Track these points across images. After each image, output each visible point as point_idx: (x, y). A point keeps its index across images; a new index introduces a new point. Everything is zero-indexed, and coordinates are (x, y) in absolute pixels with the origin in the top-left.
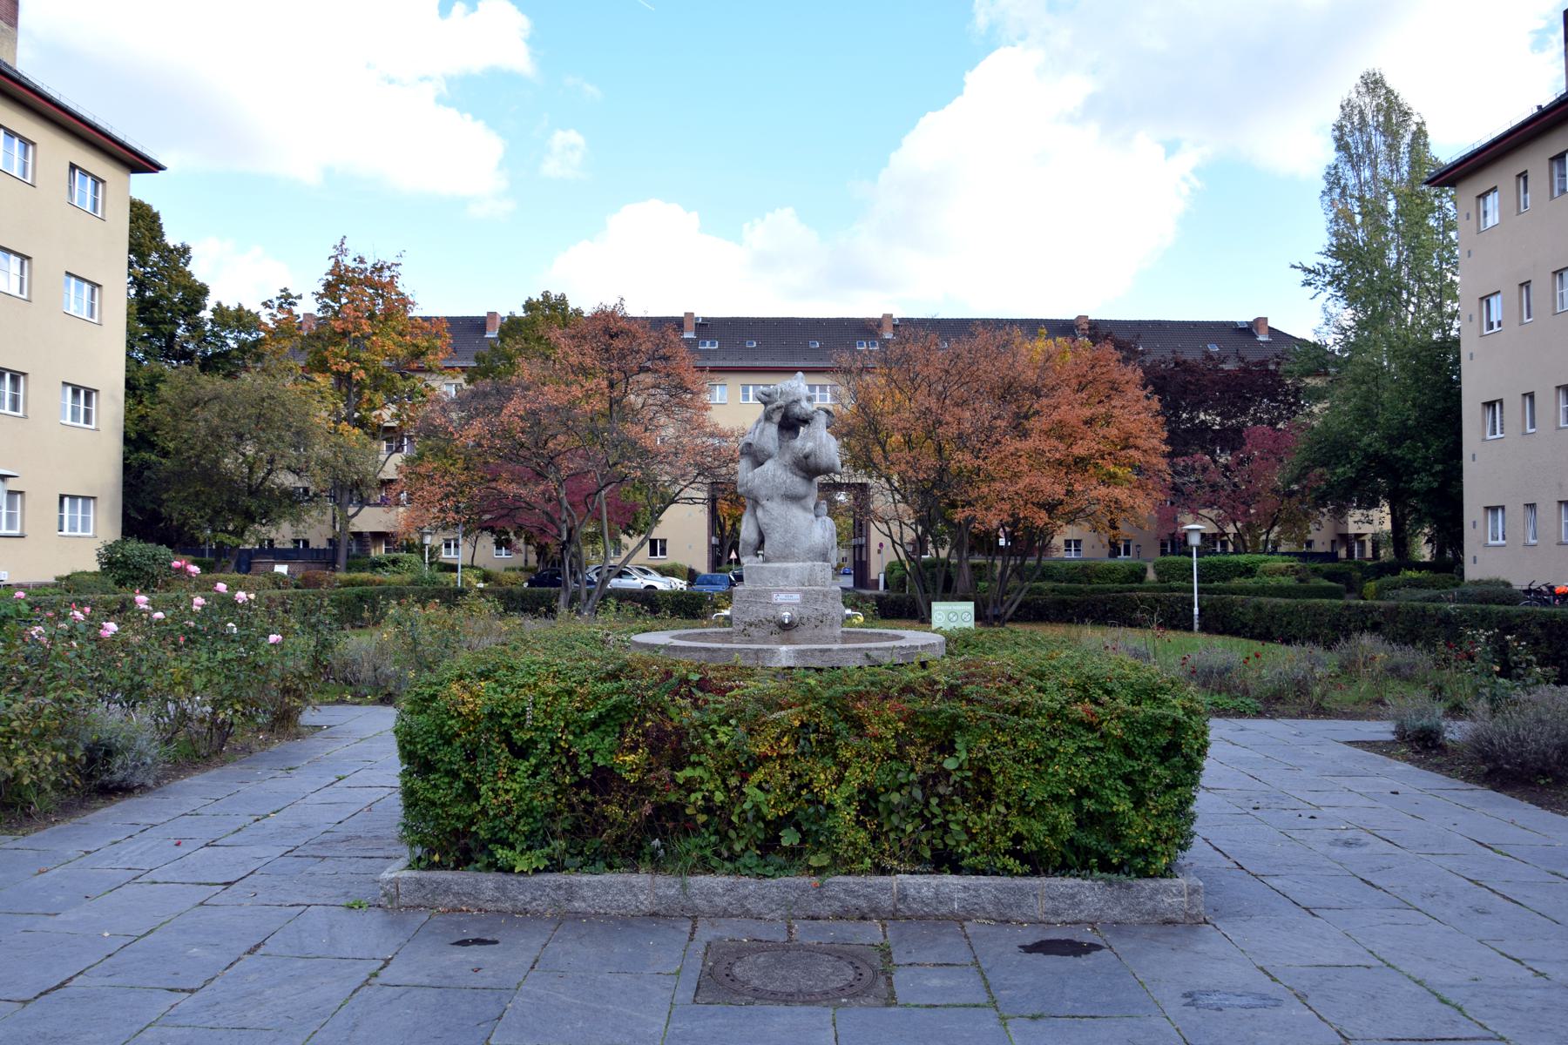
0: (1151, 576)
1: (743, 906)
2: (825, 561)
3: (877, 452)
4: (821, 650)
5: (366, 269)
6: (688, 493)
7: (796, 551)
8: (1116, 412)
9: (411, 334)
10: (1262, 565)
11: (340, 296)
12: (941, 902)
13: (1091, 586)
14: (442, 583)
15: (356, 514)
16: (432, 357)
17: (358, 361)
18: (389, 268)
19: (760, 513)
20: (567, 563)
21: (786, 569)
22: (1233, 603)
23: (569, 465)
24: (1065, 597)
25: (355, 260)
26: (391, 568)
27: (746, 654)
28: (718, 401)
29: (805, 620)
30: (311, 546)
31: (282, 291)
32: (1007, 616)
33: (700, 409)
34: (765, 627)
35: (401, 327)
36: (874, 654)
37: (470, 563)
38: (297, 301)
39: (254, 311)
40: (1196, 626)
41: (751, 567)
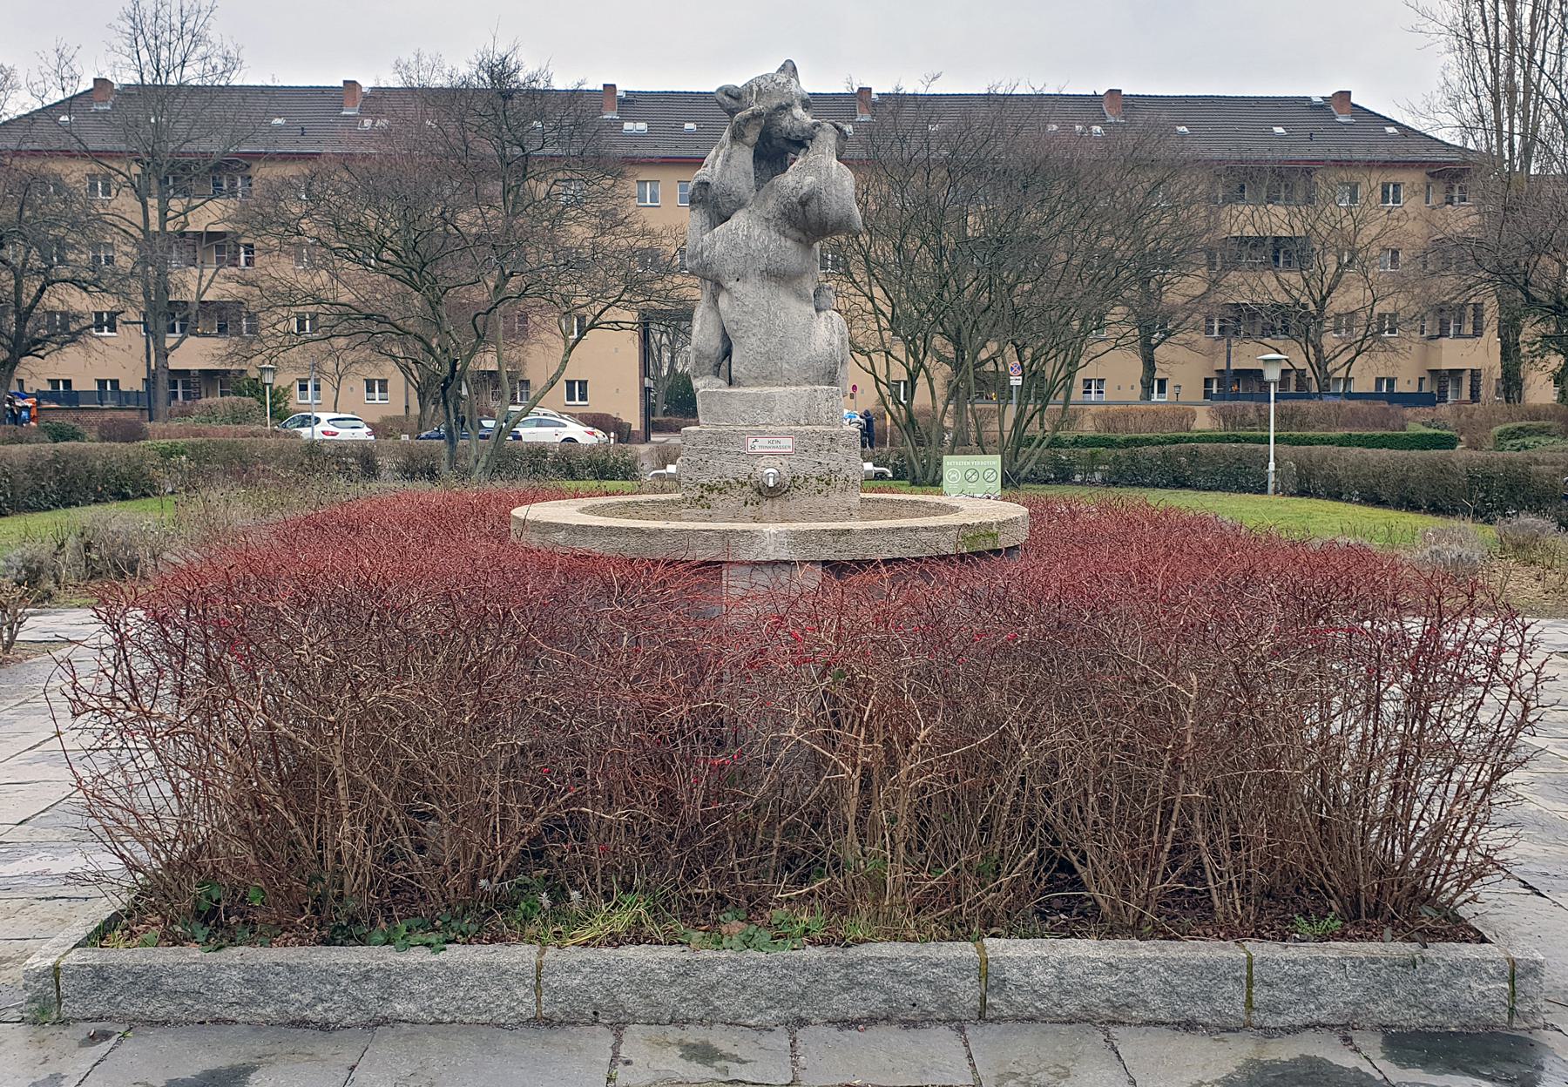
1: (706, 1002)
4: (833, 533)
12: (1067, 993)
15: (176, 346)
19: (723, 301)
21: (768, 397)
28: (649, 203)
40: (1271, 487)
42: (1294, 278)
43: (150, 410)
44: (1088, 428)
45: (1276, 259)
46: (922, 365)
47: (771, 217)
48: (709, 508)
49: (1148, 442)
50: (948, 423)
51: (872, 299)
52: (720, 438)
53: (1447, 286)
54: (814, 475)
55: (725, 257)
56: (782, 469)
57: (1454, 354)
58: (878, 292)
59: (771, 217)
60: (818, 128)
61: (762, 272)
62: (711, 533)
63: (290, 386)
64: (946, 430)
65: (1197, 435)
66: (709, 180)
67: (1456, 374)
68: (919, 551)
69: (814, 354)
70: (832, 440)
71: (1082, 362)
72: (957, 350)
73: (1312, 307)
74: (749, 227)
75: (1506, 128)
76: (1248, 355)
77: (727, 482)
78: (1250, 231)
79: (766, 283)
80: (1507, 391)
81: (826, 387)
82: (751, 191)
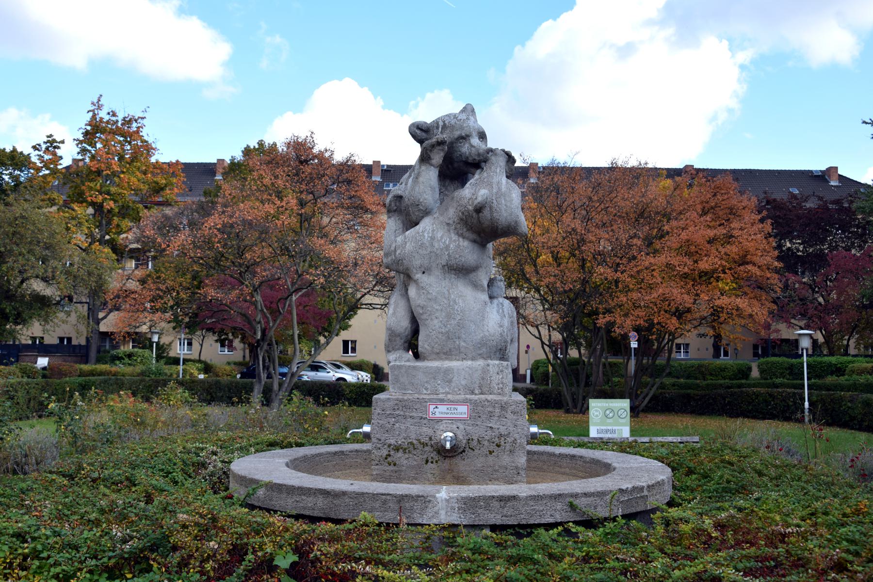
0: (755, 373)
2: (503, 358)
3: (529, 269)
5: (117, 121)
6: (368, 299)
7: (463, 344)
8: (736, 233)
9: (152, 173)
10: (851, 365)
11: (96, 142)
13: (705, 383)
14: (166, 374)
16: (168, 192)
17: (108, 193)
18: (136, 121)
19: (412, 291)
20: (261, 359)
21: (448, 371)
22: (842, 399)
23: (263, 272)
24: (689, 391)
25: (109, 114)
26: (127, 360)
27: (385, 502)
29: (474, 443)
31: (48, 137)
32: (641, 408)
33: (378, 227)
35: (144, 168)
36: (581, 503)
37: (198, 358)
38: (60, 145)
39: (26, 153)
40: (807, 419)
41: (400, 367)
47: (452, 223)
52: (403, 405)
55: (414, 254)
56: (458, 433)
59: (452, 223)
60: (490, 153)
61: (443, 266)
62: (388, 497)
63: (171, 343)
65: (753, 382)
69: (487, 334)
70: (503, 408)
74: (433, 231)
77: (411, 443)
79: (447, 275)
81: (497, 362)
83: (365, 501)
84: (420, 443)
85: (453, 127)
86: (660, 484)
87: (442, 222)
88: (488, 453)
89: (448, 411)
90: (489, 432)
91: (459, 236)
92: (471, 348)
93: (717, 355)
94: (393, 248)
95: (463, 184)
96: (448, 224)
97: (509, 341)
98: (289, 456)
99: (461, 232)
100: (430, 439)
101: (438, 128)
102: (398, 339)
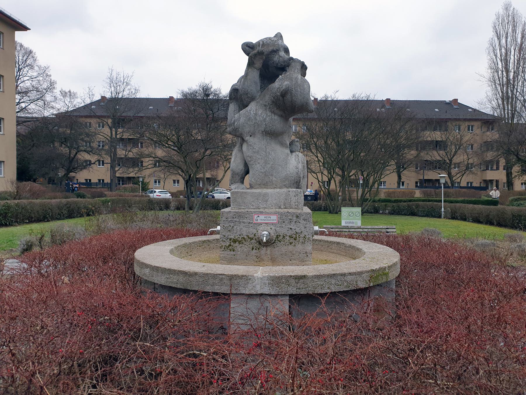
2: (298, 187)
21: (265, 195)
30: (105, 182)
34: (247, 243)
40: (443, 216)
41: (237, 193)
42: (442, 152)
43: (111, 188)
44: (382, 196)
45: (437, 147)
46: (333, 177)
47: (267, 104)
48: (234, 251)
49: (401, 201)
50: (340, 194)
51: (317, 157)
52: (240, 215)
53: (490, 155)
54: (288, 234)
55: (245, 125)
56: (271, 232)
57: (490, 175)
58: (319, 155)
59: (267, 104)
62: (224, 276)
64: (339, 196)
66: (239, 88)
67: (491, 181)
68: (346, 287)
70: (297, 217)
71: (382, 177)
72: (342, 172)
73: (448, 161)
74: (256, 110)
75: (506, 108)
76: (431, 175)
77: (243, 238)
78: (429, 139)
79: (265, 137)
80: (508, 186)
81: (295, 190)
82: (258, 92)
83: (209, 279)
84: (249, 237)
85: (268, 45)
86: (395, 264)
87: (261, 104)
88: (289, 243)
89: (265, 219)
90: (290, 231)
91: (272, 113)
92: (279, 181)
93: (399, 186)
94: (232, 122)
95: (273, 81)
96: (265, 105)
97: (302, 178)
98: (176, 244)
99: (273, 110)
100: (255, 235)
101: (259, 46)
102: (237, 176)
